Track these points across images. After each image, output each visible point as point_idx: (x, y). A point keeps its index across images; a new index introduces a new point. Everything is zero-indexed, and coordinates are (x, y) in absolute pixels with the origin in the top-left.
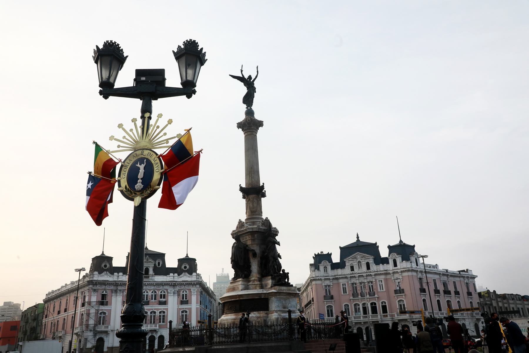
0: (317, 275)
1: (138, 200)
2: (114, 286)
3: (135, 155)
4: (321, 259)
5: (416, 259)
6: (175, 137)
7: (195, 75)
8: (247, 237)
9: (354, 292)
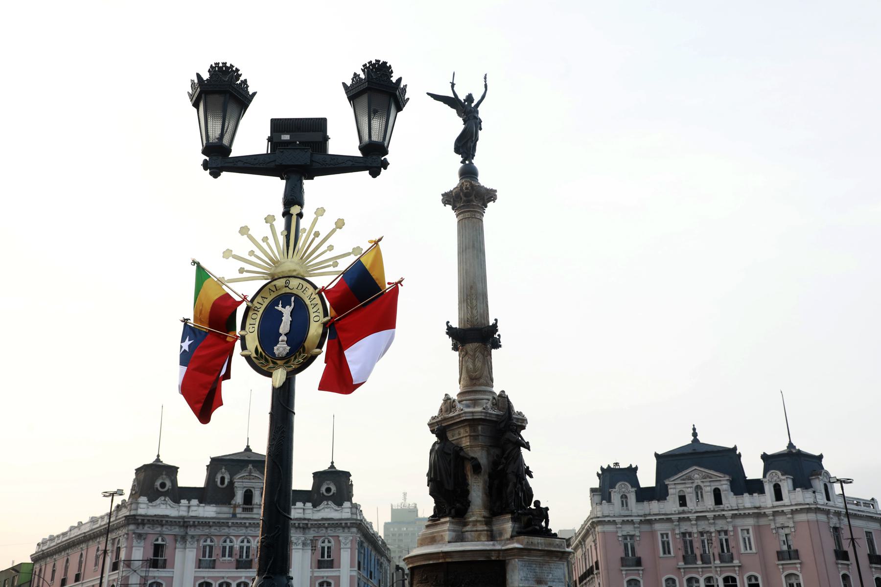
0: (606, 513)
1: (280, 375)
2: (180, 526)
3: (274, 289)
4: (615, 479)
5: (826, 486)
6: (348, 254)
7: (387, 131)
8: (462, 431)
9: (686, 552)
